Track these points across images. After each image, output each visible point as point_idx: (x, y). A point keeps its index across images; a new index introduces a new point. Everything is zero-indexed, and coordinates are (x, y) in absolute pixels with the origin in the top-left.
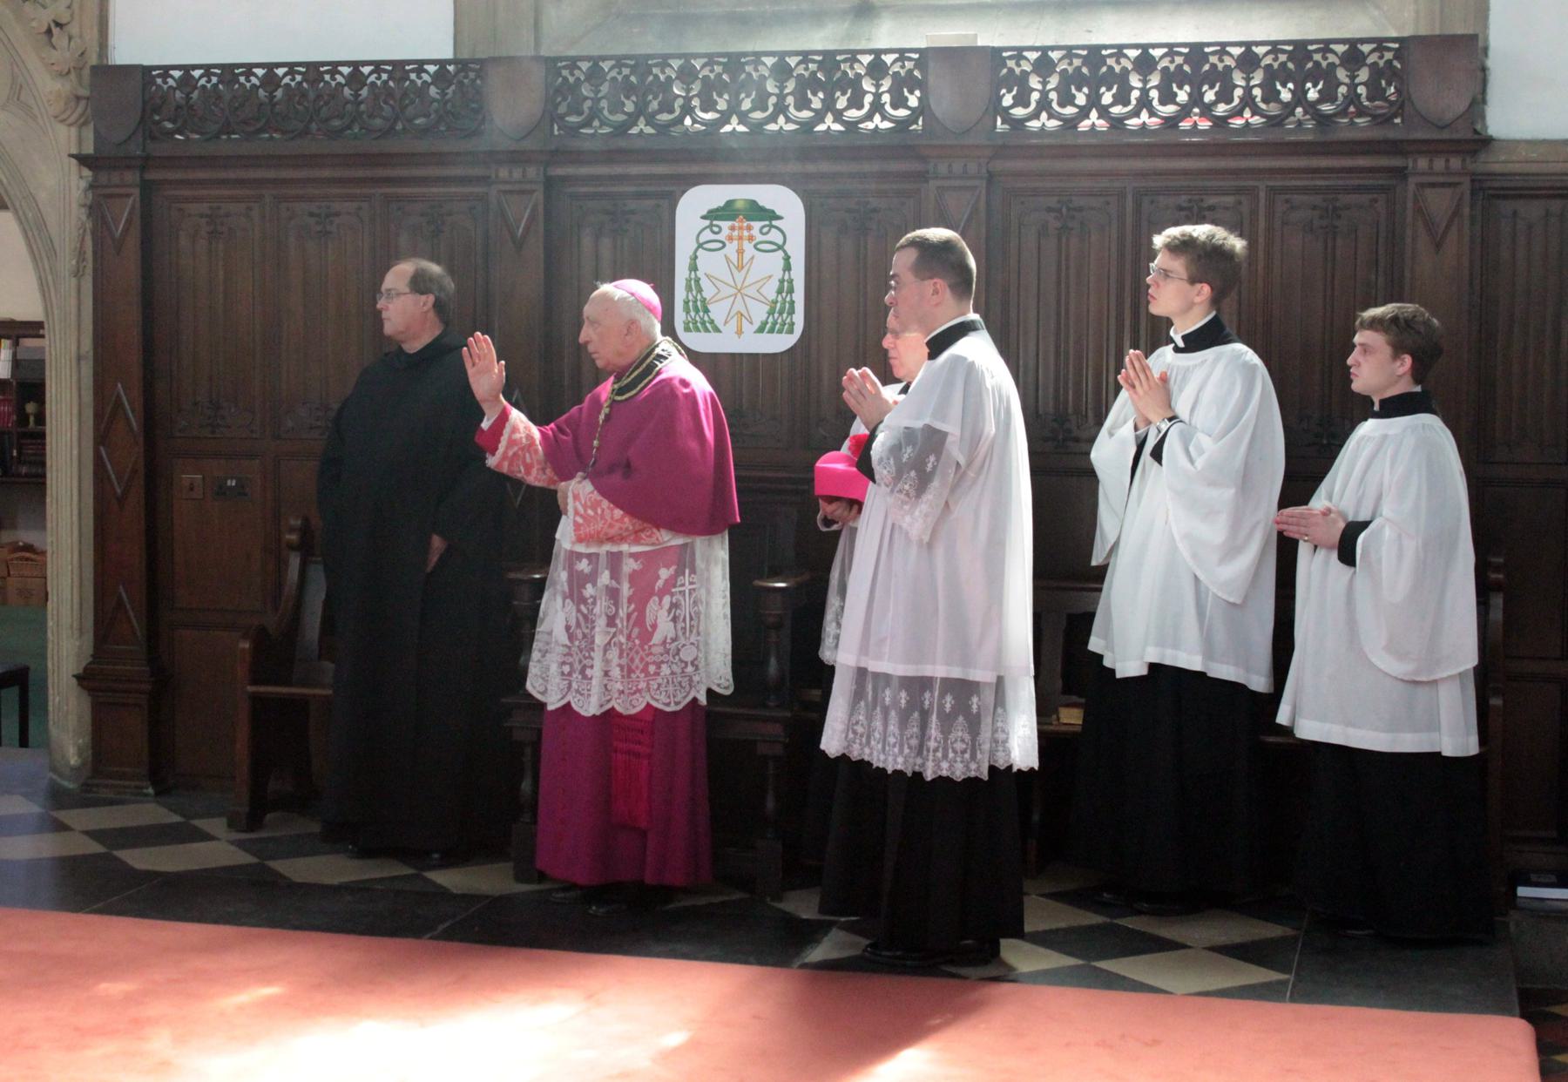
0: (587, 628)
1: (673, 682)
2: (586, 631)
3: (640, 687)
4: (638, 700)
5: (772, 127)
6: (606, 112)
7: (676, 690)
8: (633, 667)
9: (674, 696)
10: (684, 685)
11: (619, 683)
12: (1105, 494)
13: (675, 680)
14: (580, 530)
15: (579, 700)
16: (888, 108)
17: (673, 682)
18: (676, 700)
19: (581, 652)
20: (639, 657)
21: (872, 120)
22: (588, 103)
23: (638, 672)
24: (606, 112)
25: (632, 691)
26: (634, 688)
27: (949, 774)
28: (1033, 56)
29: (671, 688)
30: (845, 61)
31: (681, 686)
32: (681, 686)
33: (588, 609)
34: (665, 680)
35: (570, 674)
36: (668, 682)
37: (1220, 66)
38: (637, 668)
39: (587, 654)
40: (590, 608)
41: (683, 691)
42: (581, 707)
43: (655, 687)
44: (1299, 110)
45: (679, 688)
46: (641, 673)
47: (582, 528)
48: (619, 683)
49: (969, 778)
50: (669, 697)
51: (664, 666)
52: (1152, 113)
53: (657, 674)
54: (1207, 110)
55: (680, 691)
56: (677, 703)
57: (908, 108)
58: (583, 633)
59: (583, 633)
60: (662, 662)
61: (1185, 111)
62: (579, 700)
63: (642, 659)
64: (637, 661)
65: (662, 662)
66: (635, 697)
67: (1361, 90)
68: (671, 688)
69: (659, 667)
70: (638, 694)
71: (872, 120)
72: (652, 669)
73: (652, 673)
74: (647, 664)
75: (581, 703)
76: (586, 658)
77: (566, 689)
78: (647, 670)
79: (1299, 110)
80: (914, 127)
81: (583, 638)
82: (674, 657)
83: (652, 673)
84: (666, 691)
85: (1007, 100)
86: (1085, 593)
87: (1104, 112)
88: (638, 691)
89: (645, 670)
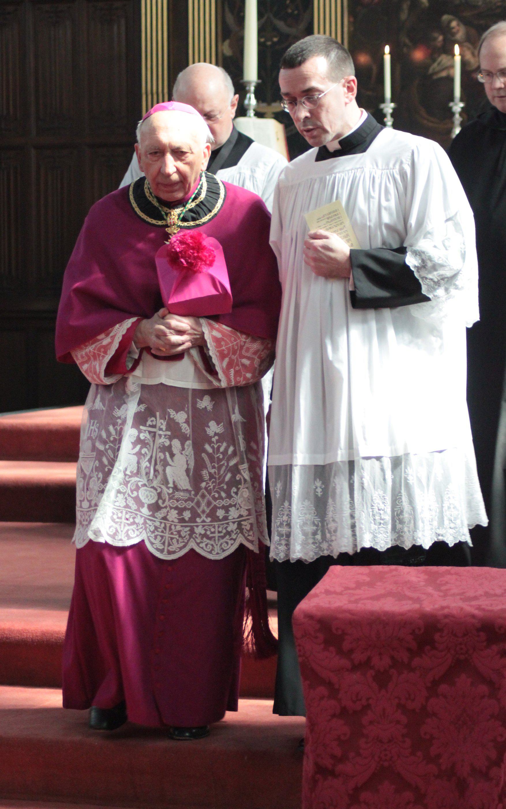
0: (214, 467)
1: (170, 529)
2: (212, 471)
3: (229, 529)
4: (227, 543)
7: (172, 539)
8: (199, 511)
9: (169, 545)
10: (183, 534)
11: (200, 527)
12: (276, 362)
13: (173, 527)
14: (222, 346)
15: (206, 545)
17: (170, 529)
18: (170, 548)
19: (210, 493)
20: (206, 500)
23: (203, 517)
25: (222, 534)
26: (224, 531)
27: (329, 554)
29: (167, 535)
31: (180, 536)
32: (180, 536)
33: (213, 448)
34: (163, 525)
35: (193, 519)
36: (165, 528)
38: (203, 512)
39: (217, 495)
40: (216, 446)
41: (180, 540)
42: (210, 552)
43: (248, 527)
45: (177, 537)
46: (206, 517)
47: (223, 343)
48: (200, 527)
49: (322, 557)
50: (164, 543)
51: (232, 509)
53: (226, 518)
55: (178, 541)
56: (170, 553)
58: (210, 473)
59: (210, 473)
60: (231, 506)
62: (206, 545)
63: (209, 504)
64: (203, 504)
65: (231, 506)
66: (225, 540)
68: (167, 535)
69: (227, 511)
70: (227, 537)
72: (220, 513)
73: (221, 518)
74: (215, 508)
75: (217, 549)
76: (215, 499)
77: (188, 537)
78: (183, 512)
81: (210, 480)
82: (132, 491)
83: (221, 518)
84: (162, 537)
88: (229, 533)
89: (212, 515)
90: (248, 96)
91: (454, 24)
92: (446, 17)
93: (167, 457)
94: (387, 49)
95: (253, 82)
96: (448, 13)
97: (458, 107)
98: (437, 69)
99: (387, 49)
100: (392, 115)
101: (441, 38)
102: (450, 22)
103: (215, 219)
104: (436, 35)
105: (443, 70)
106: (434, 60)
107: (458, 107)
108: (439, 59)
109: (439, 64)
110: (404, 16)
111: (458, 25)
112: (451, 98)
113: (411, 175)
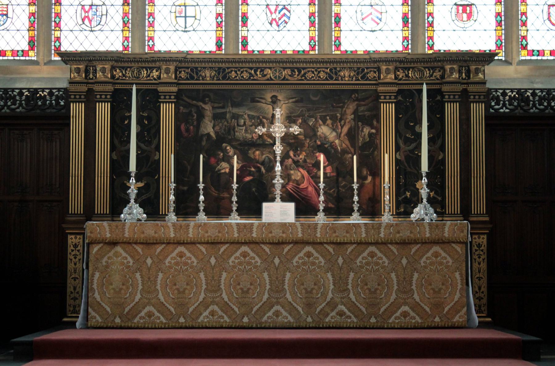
5: (502, 110)
6: (537, 105)
16: (507, 105)
21: (503, 109)
22: (18, 102)
24: (537, 105)
28: (501, 91)
30: (494, 92)
37: (43, 95)
44: (6, 108)
52: (537, 108)
54: (9, 107)
57: (544, 106)
61: (546, 108)
67: (23, 102)
71: (503, 109)
79: (6, 108)
80: (491, 110)
85: (493, 104)
86: (89, 303)
87: (9, 107)
90: (132, 178)
91: (228, 148)
92: (224, 145)
93: (122, 250)
94: (201, 156)
95: (134, 172)
96: (226, 143)
97: (235, 186)
98: (221, 168)
99: (201, 156)
100: (203, 190)
101: (222, 154)
102: (226, 147)
103: (139, 98)
104: (220, 153)
105: (223, 169)
106: (218, 165)
107: (235, 186)
108: (221, 164)
109: (220, 166)
110: (204, 143)
111: (230, 148)
112: (233, 183)
113: (513, 334)
